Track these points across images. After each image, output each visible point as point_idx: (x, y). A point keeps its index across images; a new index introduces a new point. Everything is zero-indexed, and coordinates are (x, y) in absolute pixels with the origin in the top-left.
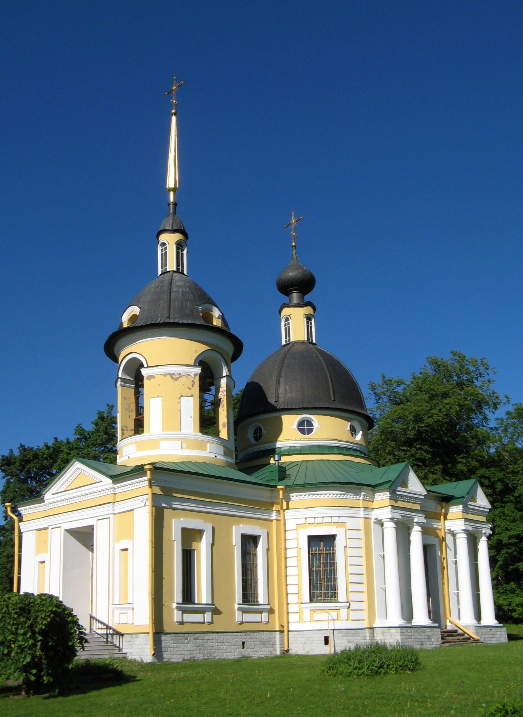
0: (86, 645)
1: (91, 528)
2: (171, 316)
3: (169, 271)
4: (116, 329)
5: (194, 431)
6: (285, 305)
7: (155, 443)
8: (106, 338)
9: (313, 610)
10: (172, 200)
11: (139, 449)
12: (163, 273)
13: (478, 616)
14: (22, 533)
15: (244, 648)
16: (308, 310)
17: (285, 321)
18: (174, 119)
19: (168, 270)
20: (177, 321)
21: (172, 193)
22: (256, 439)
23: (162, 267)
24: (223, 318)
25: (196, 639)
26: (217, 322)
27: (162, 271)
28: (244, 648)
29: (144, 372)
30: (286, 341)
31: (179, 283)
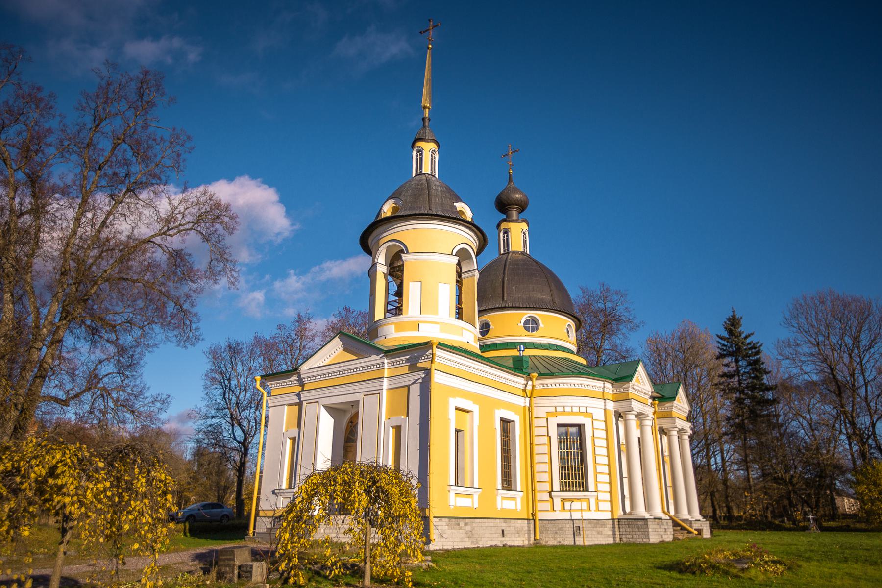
0: (237, 220)
3: (424, 174)
6: (505, 220)
11: (397, 330)
12: (417, 175)
13: (648, 506)
14: (610, 501)
15: (503, 536)
16: (524, 226)
17: (504, 233)
19: (423, 172)
23: (416, 170)
25: (466, 525)
26: (470, 220)
27: (416, 174)
28: (503, 536)
29: (405, 257)
30: (504, 251)
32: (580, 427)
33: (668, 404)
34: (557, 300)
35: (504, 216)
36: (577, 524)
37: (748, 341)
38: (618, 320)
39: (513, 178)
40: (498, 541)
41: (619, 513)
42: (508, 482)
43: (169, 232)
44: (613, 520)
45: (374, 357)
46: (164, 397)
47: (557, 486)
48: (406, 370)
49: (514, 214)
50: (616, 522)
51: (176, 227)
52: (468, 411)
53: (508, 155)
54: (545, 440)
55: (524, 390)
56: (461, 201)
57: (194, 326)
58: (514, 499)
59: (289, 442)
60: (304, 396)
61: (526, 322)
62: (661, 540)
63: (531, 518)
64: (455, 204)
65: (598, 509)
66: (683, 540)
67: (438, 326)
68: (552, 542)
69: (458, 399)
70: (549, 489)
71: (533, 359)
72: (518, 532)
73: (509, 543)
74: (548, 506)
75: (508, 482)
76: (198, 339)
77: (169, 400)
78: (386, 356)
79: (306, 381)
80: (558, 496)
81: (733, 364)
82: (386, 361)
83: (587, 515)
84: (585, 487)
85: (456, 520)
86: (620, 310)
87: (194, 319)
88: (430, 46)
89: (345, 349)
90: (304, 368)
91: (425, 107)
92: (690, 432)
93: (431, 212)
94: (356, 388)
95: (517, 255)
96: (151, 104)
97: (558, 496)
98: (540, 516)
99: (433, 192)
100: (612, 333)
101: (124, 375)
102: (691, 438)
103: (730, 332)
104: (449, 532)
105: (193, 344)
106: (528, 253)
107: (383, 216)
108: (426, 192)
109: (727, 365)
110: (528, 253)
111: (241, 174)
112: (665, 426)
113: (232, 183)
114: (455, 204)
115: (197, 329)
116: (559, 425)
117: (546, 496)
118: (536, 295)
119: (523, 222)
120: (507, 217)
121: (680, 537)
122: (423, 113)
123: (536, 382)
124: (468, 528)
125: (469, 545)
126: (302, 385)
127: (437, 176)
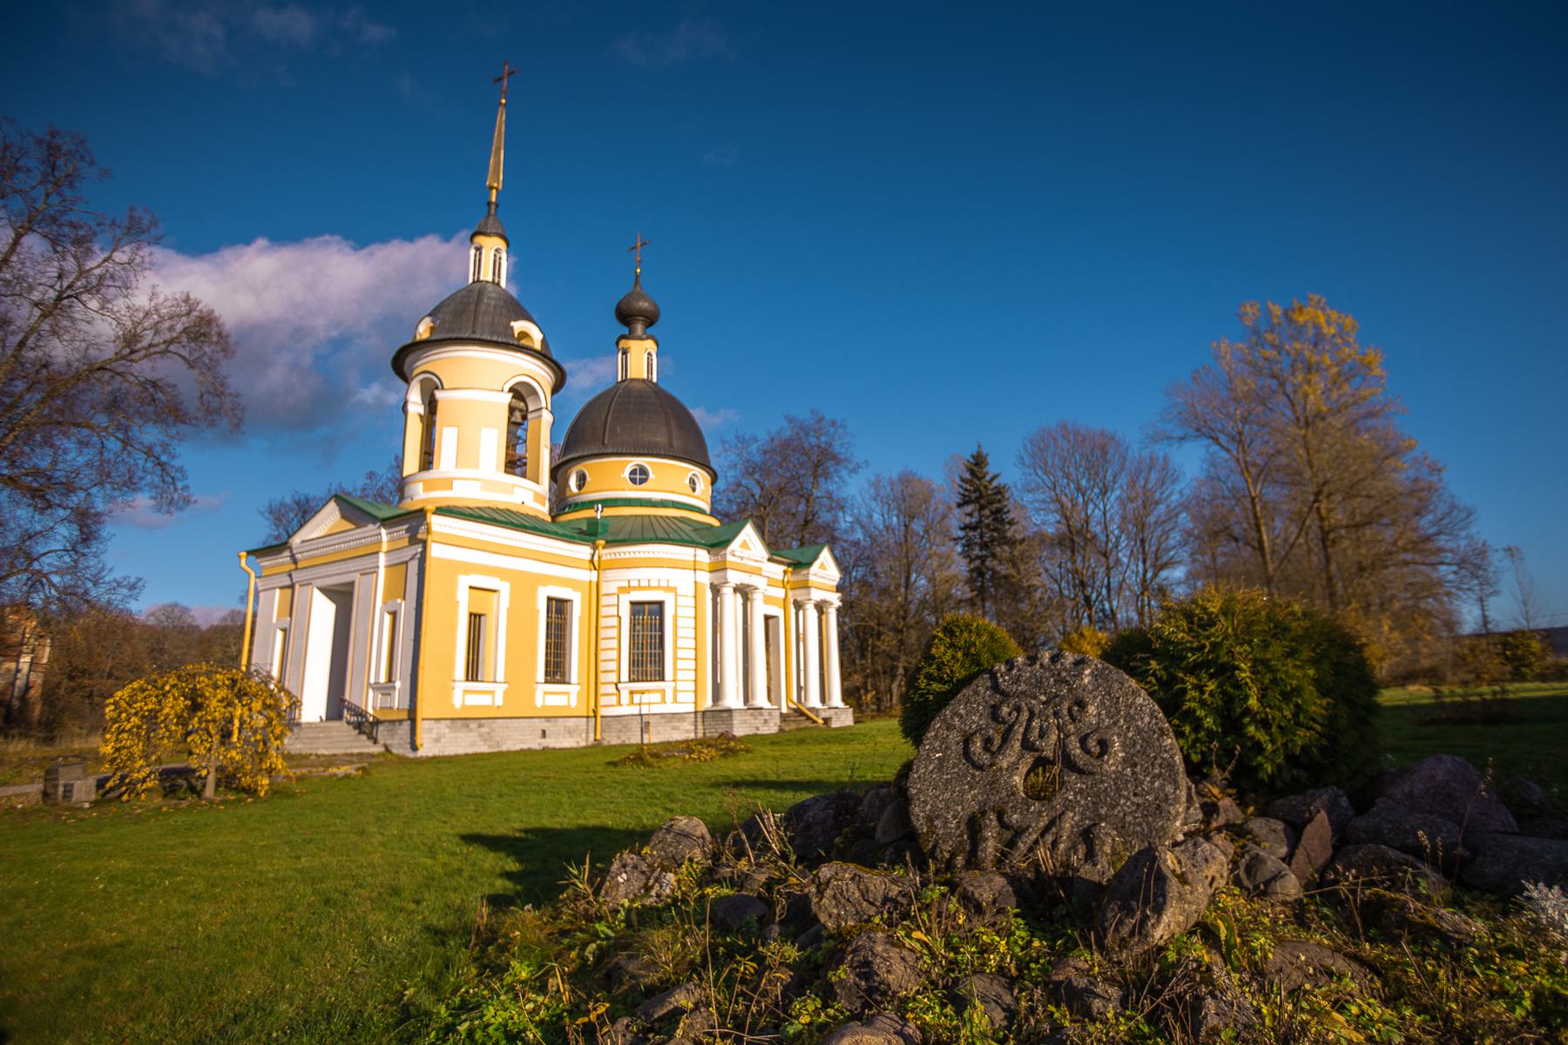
1: (352, 584)
2: (478, 331)
4: (409, 341)
5: (497, 469)
6: (623, 337)
7: (448, 483)
8: (393, 353)
9: (466, 692)
10: (494, 199)
11: (427, 488)
16: (650, 345)
18: (502, 117)
20: (484, 337)
21: (494, 191)
22: (580, 487)
24: (544, 341)
25: (480, 726)
26: (538, 346)
29: (439, 394)
31: (493, 295)
32: (661, 604)
33: (805, 572)
34: (676, 443)
35: (626, 331)
36: (645, 719)
37: (995, 483)
38: (837, 460)
39: (641, 280)
40: (535, 743)
41: (708, 703)
42: (556, 670)
43: (133, 357)
44: (696, 712)
45: (371, 526)
46: (132, 580)
47: (625, 676)
48: (405, 542)
49: (639, 328)
50: (699, 715)
51: (144, 348)
52: (495, 591)
53: (635, 248)
54: (614, 621)
55: (592, 561)
56: (530, 319)
57: (180, 485)
58: (492, 692)
59: (279, 635)
60: (297, 576)
61: (633, 472)
62: (755, 732)
63: (592, 714)
64: (513, 324)
65: (675, 701)
66: (790, 731)
67: (479, 483)
68: (615, 741)
69: (472, 576)
70: (615, 679)
71: (653, 520)
72: (570, 732)
73: (551, 746)
74: (614, 700)
75: (556, 670)
76: (187, 501)
77: (140, 584)
78: (385, 527)
79: (299, 556)
80: (626, 687)
81: (976, 514)
82: (383, 531)
83: (656, 709)
84: (661, 677)
85: (462, 721)
86: (837, 448)
87: (179, 475)
88: (503, 101)
89: (344, 517)
90: (296, 541)
91: (491, 188)
92: (838, 603)
93: (473, 336)
94: (351, 565)
95: (636, 383)
96: (70, 179)
97: (626, 687)
98: (603, 712)
99: (483, 308)
100: (827, 476)
101: (76, 552)
102: (838, 610)
103: (973, 473)
104: (452, 735)
105: (181, 509)
106: (655, 380)
107: (418, 338)
108: (472, 307)
109: (970, 515)
110: (655, 380)
111: (395, 237)
112: (799, 599)
113: (364, 252)
114: (513, 324)
115: (186, 488)
116: (632, 603)
117: (612, 689)
118: (661, 439)
119: (647, 338)
120: (630, 332)
121: (787, 729)
122: (490, 195)
123: (604, 552)
124: (483, 730)
125: (484, 749)
126: (295, 562)
127: (503, 284)
